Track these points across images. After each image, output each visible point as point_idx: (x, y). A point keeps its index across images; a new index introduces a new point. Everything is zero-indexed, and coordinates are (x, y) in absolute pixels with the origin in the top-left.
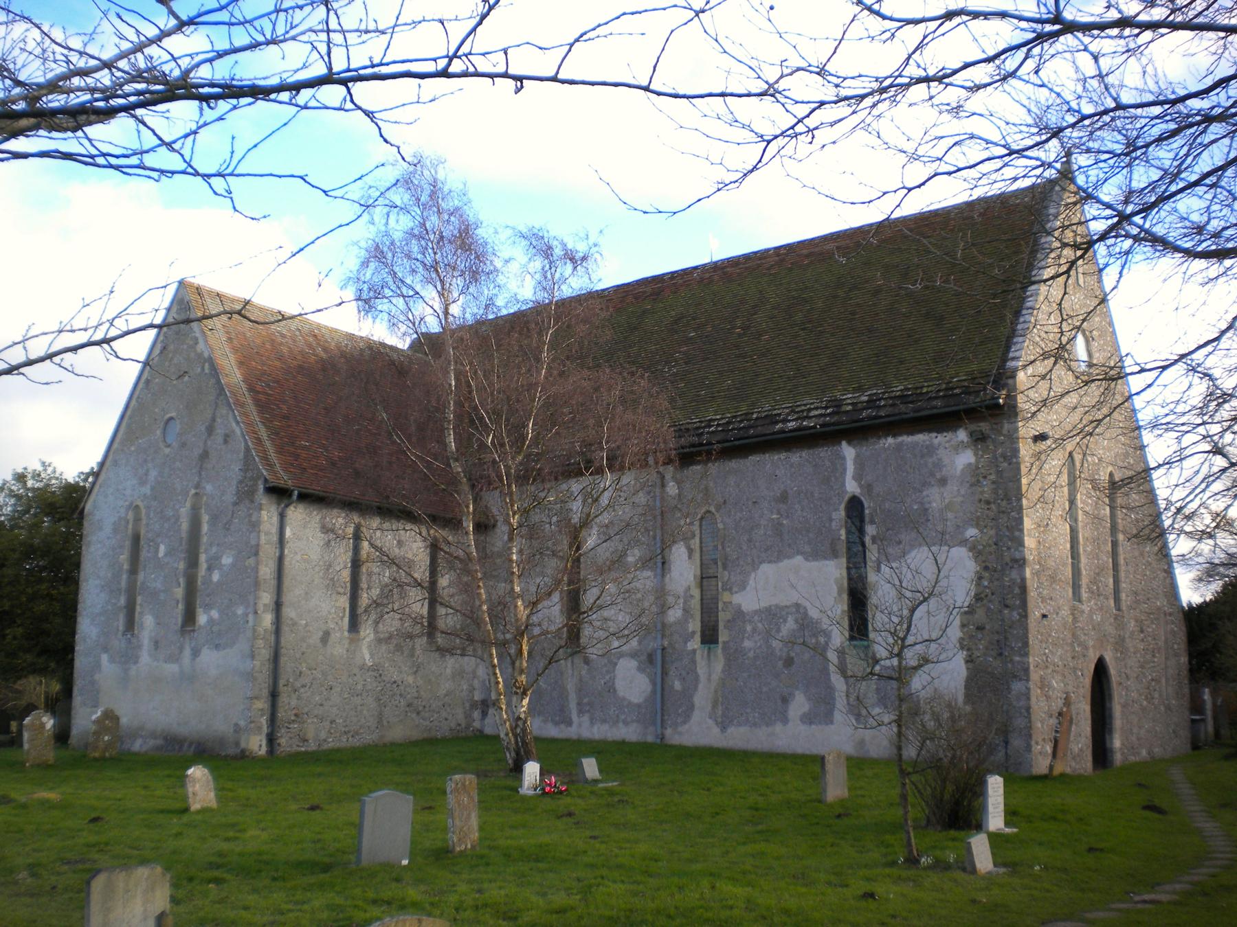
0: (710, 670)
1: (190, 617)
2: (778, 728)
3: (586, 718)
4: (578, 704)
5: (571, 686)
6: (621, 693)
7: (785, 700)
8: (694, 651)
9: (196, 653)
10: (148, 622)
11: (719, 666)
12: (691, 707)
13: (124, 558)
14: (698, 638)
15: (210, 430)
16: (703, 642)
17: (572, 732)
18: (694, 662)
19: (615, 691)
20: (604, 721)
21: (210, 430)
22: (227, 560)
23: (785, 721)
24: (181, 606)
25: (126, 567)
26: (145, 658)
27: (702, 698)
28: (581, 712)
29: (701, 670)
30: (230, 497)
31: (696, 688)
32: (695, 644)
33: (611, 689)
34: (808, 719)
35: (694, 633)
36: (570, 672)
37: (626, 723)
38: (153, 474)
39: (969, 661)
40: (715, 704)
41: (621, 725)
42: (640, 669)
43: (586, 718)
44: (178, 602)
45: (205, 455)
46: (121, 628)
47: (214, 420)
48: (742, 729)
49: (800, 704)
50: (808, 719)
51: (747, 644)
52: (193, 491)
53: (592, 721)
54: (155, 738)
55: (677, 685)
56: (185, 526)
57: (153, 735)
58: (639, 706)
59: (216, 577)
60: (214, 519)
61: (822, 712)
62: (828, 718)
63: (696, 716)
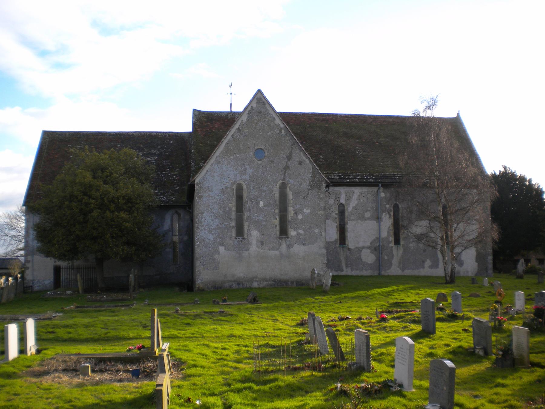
0: (397, 253)
1: (284, 232)
2: (421, 270)
3: (349, 269)
4: (346, 264)
5: (342, 258)
6: (364, 260)
7: (424, 262)
8: (392, 247)
9: (289, 246)
10: (255, 234)
11: (401, 251)
12: (391, 264)
13: (232, 205)
14: (393, 243)
15: (289, 158)
16: (395, 244)
17: (343, 273)
18: (392, 250)
19: (361, 260)
20: (357, 270)
21: (289, 158)
22: (306, 211)
23: (423, 267)
24: (278, 228)
25: (234, 209)
26: (254, 248)
27: (395, 261)
28: (347, 267)
29: (395, 252)
30: (305, 186)
31: (393, 259)
32: (392, 245)
33: (360, 258)
34: (431, 267)
35: (392, 241)
36: (342, 253)
37: (366, 270)
38: (250, 171)
39: (477, 251)
40: (400, 263)
41: (364, 271)
42: (371, 252)
43: (349, 269)
44: (276, 226)
45: (287, 168)
46: (234, 235)
47: (291, 154)
48: (409, 271)
49: (428, 263)
50: (431, 267)
51: (411, 245)
52: (281, 181)
53: (352, 270)
54: (267, 281)
55: (386, 258)
56: (277, 195)
57: (265, 280)
58: (371, 264)
59: (300, 217)
60: (296, 194)
61: (435, 265)
62: (437, 266)
63: (393, 267)
